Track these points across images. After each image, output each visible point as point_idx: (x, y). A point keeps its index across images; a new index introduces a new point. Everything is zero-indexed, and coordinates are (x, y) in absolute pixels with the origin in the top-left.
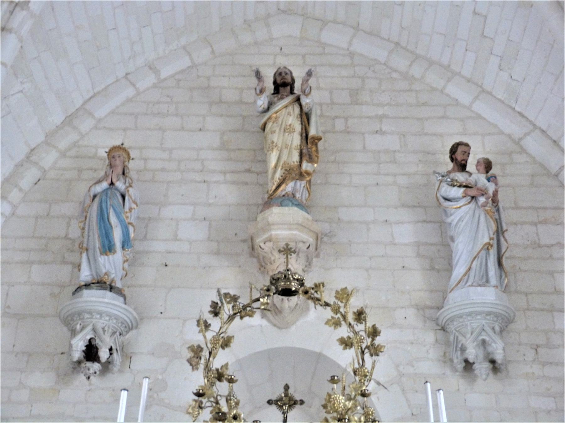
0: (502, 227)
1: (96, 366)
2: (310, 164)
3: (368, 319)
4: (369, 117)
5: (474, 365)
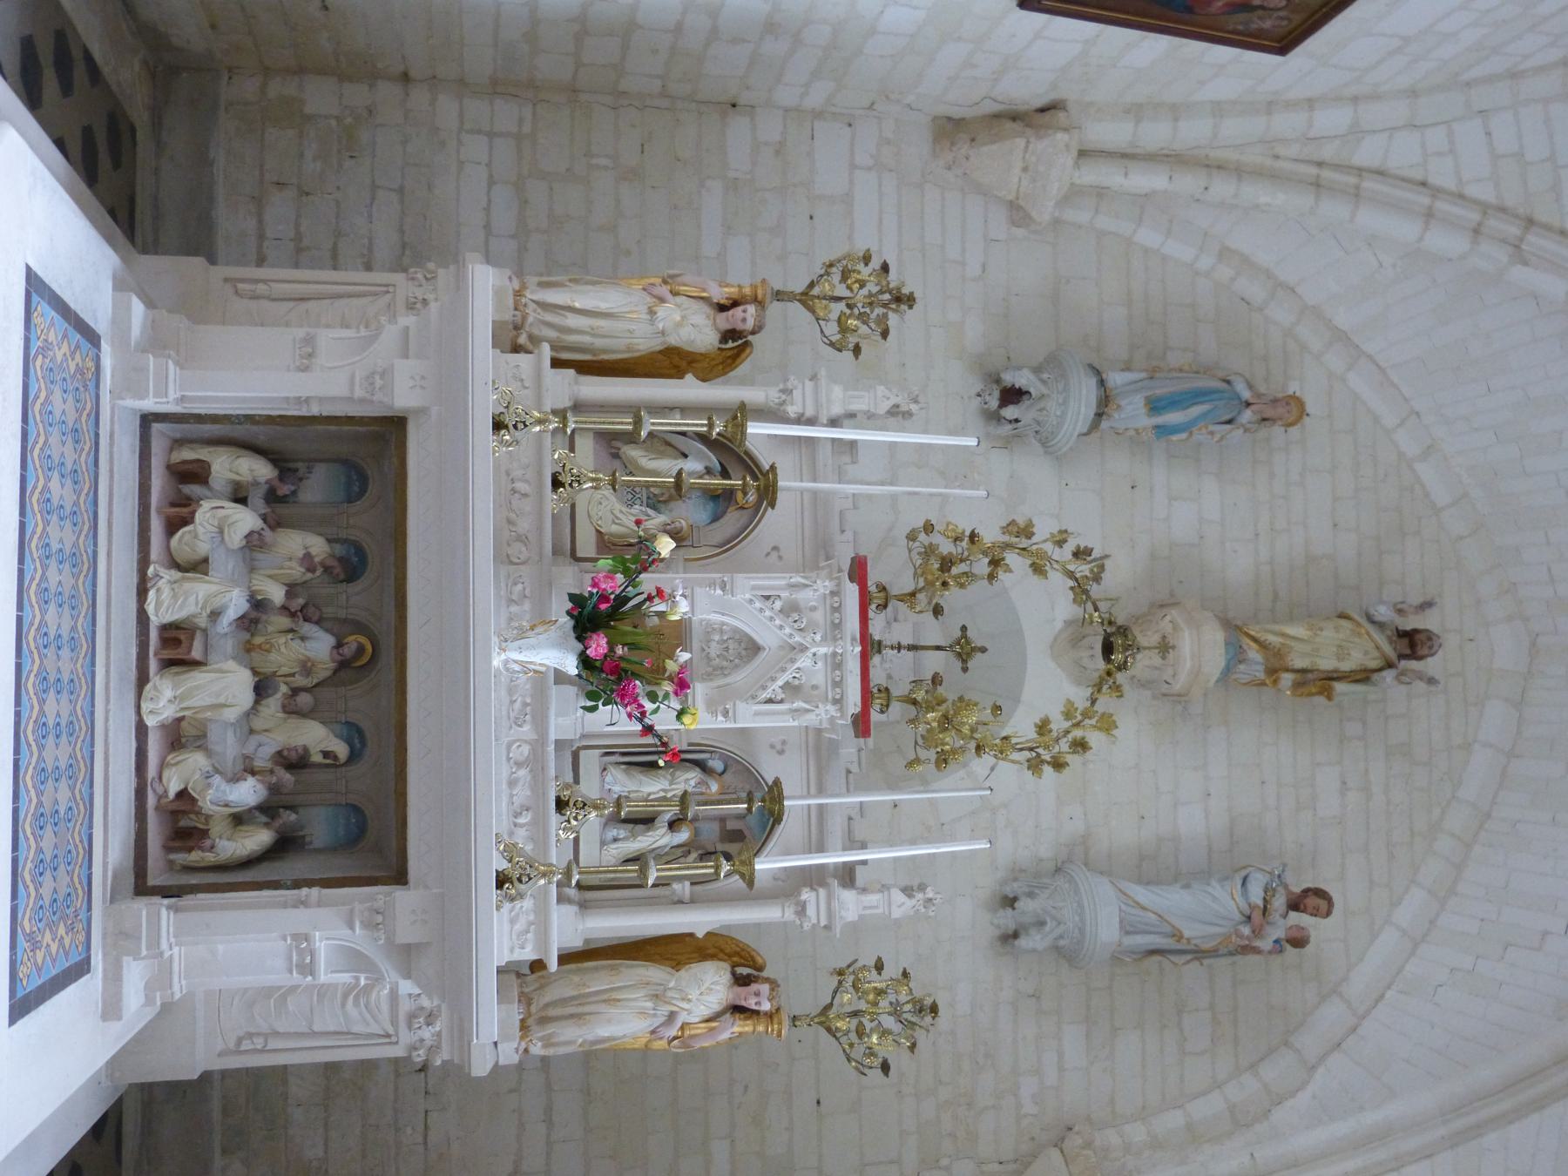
0: (1206, 957)
1: (994, 403)
2: (1290, 684)
3: (1076, 756)
4: (1367, 771)
5: (1010, 910)
